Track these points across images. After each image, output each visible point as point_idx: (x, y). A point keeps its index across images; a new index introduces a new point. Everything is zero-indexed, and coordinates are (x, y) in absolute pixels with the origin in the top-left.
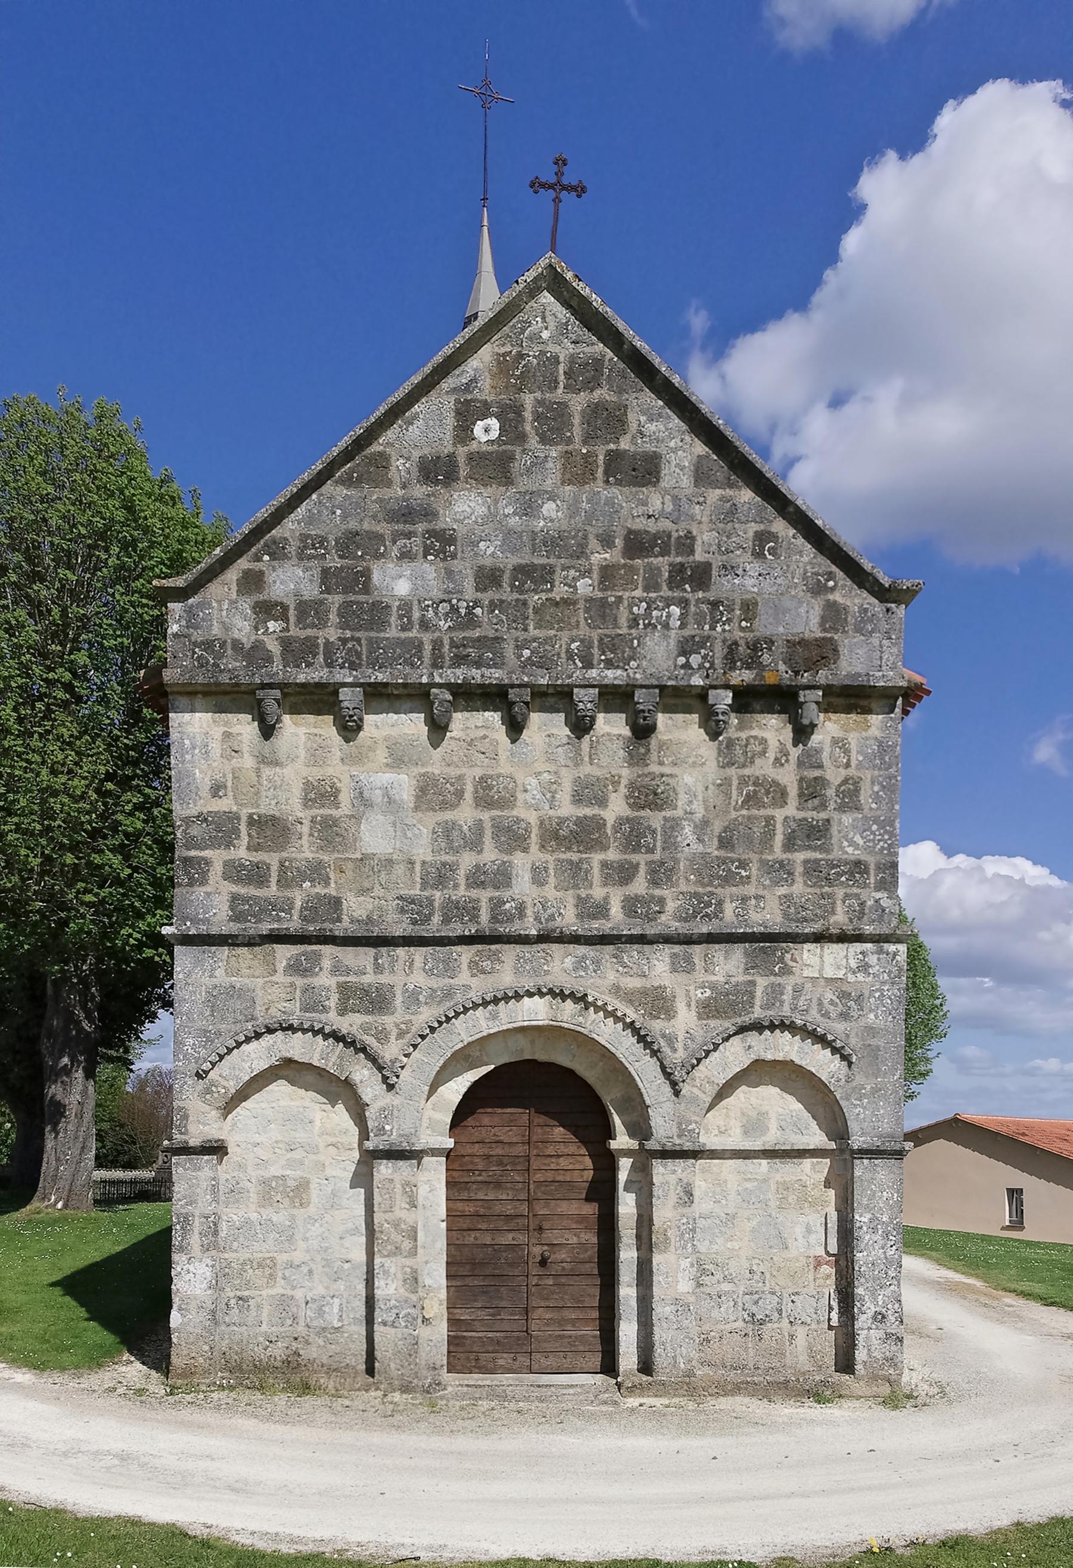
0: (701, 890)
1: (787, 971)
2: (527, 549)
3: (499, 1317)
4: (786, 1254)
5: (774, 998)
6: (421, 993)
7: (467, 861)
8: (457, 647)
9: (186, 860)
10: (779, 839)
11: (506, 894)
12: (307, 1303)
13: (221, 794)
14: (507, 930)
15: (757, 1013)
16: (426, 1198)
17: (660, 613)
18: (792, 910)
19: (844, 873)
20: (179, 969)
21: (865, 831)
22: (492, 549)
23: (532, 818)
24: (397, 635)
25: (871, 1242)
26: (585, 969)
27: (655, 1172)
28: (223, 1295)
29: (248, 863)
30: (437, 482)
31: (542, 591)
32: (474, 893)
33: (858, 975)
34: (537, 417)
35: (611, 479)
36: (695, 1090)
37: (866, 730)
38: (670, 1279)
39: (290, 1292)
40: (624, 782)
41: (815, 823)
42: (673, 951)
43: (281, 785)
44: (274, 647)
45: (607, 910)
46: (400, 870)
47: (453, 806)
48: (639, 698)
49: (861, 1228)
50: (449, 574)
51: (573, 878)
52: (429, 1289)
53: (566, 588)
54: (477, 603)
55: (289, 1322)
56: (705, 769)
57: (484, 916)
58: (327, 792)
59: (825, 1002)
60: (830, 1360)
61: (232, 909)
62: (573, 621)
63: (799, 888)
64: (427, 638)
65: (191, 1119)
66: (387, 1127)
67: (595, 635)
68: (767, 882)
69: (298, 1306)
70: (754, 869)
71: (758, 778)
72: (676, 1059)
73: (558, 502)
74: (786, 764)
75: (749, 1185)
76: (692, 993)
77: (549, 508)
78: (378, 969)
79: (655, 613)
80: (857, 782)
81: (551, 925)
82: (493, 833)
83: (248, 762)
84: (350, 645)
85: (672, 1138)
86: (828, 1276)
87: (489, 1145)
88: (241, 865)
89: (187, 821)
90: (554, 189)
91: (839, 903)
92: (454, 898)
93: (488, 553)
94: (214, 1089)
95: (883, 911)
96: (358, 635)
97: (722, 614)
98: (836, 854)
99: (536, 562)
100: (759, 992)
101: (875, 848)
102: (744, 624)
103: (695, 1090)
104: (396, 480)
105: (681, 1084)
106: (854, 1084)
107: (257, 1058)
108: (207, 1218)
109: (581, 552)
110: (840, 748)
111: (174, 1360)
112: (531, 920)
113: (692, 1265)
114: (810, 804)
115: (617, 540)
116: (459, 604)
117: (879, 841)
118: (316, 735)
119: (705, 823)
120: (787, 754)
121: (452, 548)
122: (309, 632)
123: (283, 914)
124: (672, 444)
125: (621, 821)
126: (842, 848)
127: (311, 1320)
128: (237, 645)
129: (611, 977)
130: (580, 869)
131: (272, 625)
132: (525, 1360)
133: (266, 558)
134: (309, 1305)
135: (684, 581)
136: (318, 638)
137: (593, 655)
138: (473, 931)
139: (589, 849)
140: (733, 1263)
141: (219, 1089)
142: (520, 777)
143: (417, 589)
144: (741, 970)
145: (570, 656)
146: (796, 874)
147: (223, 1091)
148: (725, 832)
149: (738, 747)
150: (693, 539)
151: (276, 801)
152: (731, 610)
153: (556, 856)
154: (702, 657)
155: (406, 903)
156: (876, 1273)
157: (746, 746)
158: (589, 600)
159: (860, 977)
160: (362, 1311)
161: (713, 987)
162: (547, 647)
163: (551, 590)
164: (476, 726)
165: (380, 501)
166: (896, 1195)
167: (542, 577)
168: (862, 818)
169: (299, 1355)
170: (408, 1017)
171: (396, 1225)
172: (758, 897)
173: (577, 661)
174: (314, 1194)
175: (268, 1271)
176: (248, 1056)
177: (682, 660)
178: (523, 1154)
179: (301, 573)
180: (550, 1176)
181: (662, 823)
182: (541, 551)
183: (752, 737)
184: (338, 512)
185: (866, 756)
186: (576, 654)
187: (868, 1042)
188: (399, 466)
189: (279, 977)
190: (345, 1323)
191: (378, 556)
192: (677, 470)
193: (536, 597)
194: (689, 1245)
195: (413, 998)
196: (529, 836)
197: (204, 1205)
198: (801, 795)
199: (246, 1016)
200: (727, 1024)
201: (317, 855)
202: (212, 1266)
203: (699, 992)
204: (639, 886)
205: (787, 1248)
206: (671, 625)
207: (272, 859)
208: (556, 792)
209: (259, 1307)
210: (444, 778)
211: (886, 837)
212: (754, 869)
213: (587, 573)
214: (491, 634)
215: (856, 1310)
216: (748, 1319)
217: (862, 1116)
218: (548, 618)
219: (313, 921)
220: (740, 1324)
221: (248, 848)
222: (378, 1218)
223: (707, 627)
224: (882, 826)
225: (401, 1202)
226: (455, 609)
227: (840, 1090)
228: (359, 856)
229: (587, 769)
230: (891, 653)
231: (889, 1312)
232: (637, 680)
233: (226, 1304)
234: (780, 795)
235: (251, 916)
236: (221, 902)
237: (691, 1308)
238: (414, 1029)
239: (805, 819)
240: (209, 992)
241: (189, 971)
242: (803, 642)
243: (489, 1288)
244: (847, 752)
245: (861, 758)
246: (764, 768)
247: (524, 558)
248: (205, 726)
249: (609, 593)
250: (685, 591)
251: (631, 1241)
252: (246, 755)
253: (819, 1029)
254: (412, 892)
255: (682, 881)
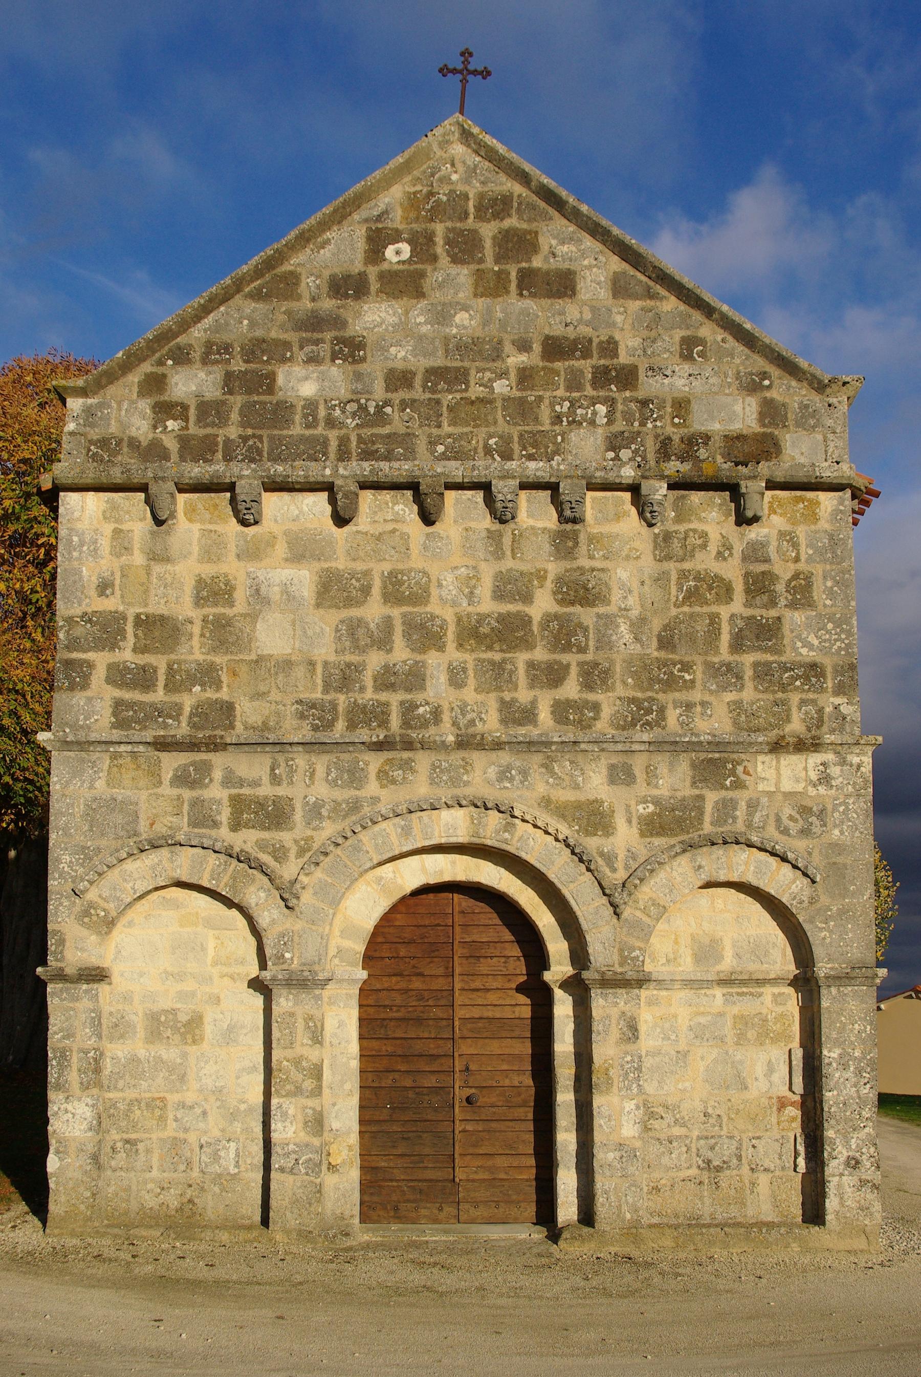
0: (639, 695)
1: (739, 785)
2: (440, 353)
3: (421, 1165)
4: (747, 1095)
5: (727, 815)
6: (323, 806)
7: (375, 660)
8: (365, 444)
9: (68, 663)
10: (725, 638)
11: (419, 697)
12: (201, 1147)
13: (108, 592)
14: (420, 736)
15: (707, 828)
16: (335, 1035)
17: (584, 412)
18: (743, 718)
19: (798, 677)
20: (55, 779)
21: (819, 630)
22: (403, 353)
23: (449, 615)
24: (302, 432)
25: (842, 1080)
26: (511, 779)
27: (594, 1005)
28: (108, 1138)
29: (134, 666)
30: (347, 296)
31: (456, 391)
32: (383, 696)
33: (819, 788)
34: (448, 242)
35: (524, 292)
36: (638, 914)
37: (815, 523)
38: (613, 1123)
39: (181, 1135)
40: (551, 577)
41: (764, 621)
42: (610, 761)
43: (172, 583)
44: (172, 445)
45: (535, 715)
46: (300, 672)
47: (360, 603)
48: (565, 489)
49: (830, 1064)
50: (358, 376)
51: (495, 679)
52: (337, 1134)
53: (481, 388)
54: (387, 403)
55: (182, 1167)
56: (642, 562)
57: (395, 722)
58: (221, 589)
59: (784, 819)
60: (797, 1211)
61: (114, 714)
62: (490, 418)
63: (748, 694)
64: (333, 436)
65: (67, 944)
66: (288, 955)
67: (515, 432)
68: (714, 687)
69: (192, 1150)
70: (699, 669)
71: (699, 572)
72: (616, 879)
73: (471, 312)
74: (730, 558)
75: (702, 1020)
76: (633, 808)
77: (462, 318)
78: (275, 780)
79: (579, 411)
80: (808, 578)
81: (471, 730)
82: (403, 631)
83: (138, 559)
84: (251, 443)
85: (613, 966)
86: (793, 1119)
87: (407, 978)
88: (127, 668)
89: (70, 620)
90: (462, 74)
91: (794, 710)
92: (360, 702)
93: (399, 356)
94: (93, 911)
95: (844, 718)
96: (258, 432)
97: (652, 411)
98: (788, 656)
99: (449, 365)
100: (709, 807)
101: (831, 648)
102: (676, 420)
103: (638, 914)
104: (306, 295)
105: (623, 906)
106: (818, 905)
107: (140, 878)
108: (86, 1053)
109: (497, 354)
110: (788, 541)
111: (52, 1207)
112: (448, 725)
113: (638, 1108)
114: (758, 600)
115: (534, 346)
116: (368, 404)
117: (836, 640)
118: (211, 531)
119: (643, 620)
120: (730, 548)
121: (361, 353)
122: (209, 431)
123: (170, 721)
124: (586, 262)
125: (548, 619)
126: (795, 649)
127: (206, 1166)
128: (134, 444)
129: (541, 789)
130: (504, 670)
131: (171, 424)
132: (449, 1210)
133: (170, 362)
134: (204, 1149)
135: (609, 381)
136: (217, 436)
137: (512, 450)
138: (381, 737)
139: (512, 648)
140: (685, 1106)
141: (99, 911)
142: (434, 571)
143: (324, 390)
144: (688, 783)
145: (488, 451)
146: (746, 678)
147: (103, 914)
148: (665, 631)
149: (676, 541)
150: (616, 343)
151: (165, 599)
152: (661, 407)
153: (474, 656)
154: (633, 452)
155: (306, 709)
156: (848, 1113)
157: (685, 539)
158: (506, 399)
159: (822, 790)
160: (260, 1157)
161: (656, 802)
162: (462, 443)
163: (466, 390)
164: (385, 520)
165: (288, 313)
166: (869, 1027)
167: (456, 378)
168: (816, 616)
169: (194, 1204)
170: (309, 833)
171: (297, 1062)
172: (703, 704)
173: (496, 456)
174: (208, 1029)
175: (158, 1112)
176: (130, 876)
177: (611, 455)
178: (446, 988)
179: (204, 376)
180: (476, 1013)
181: (595, 619)
182: (455, 355)
183: (691, 530)
184: (246, 322)
185: (817, 550)
186: (494, 450)
187: (834, 860)
188: (309, 283)
189: (166, 790)
190: (242, 1169)
191: (284, 360)
192: (593, 285)
193: (450, 397)
194: (634, 1085)
195: (315, 812)
196: (445, 634)
197: (84, 1038)
198: (748, 591)
199: (128, 831)
200: (673, 841)
201: (209, 657)
202: (93, 1106)
203: (640, 807)
204: (571, 689)
205: (746, 1088)
206: (597, 422)
207: (160, 662)
208: (474, 587)
209: (148, 1151)
210: (349, 574)
211: (843, 636)
212: (699, 669)
213: (503, 374)
214: (402, 430)
215: (826, 1154)
216: (703, 1165)
217: (828, 940)
218: (463, 415)
219: (202, 728)
220: (694, 1171)
221: (135, 650)
222: (276, 1054)
223: (636, 424)
224: (838, 624)
225: (302, 1037)
226: (363, 408)
227: (803, 913)
228: (253, 657)
229: (509, 563)
230: (838, 445)
231: (864, 1157)
232: (561, 471)
233: (112, 1147)
234: (725, 592)
235: (135, 722)
236: (103, 708)
237: (638, 1154)
238: (315, 846)
239: (754, 617)
240: (88, 805)
241: (66, 782)
242: (740, 437)
243: (410, 1135)
244: (795, 546)
245: (811, 552)
246: (705, 562)
247: (439, 361)
248: (95, 522)
249: (529, 393)
250: (611, 390)
251: (568, 1082)
252: (137, 552)
253: (777, 847)
254: (314, 696)
255: (618, 684)
